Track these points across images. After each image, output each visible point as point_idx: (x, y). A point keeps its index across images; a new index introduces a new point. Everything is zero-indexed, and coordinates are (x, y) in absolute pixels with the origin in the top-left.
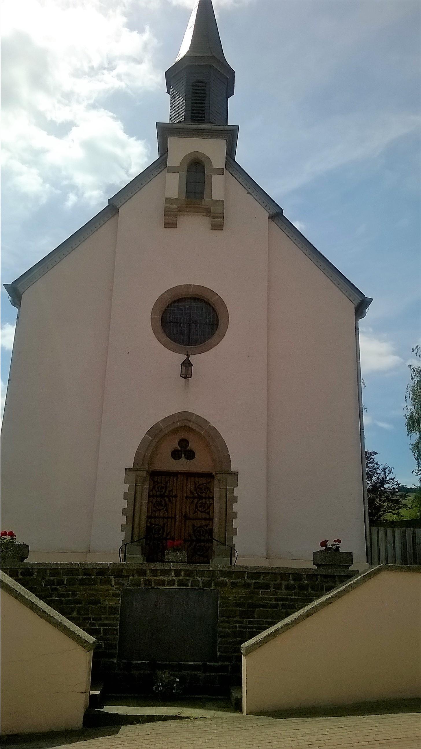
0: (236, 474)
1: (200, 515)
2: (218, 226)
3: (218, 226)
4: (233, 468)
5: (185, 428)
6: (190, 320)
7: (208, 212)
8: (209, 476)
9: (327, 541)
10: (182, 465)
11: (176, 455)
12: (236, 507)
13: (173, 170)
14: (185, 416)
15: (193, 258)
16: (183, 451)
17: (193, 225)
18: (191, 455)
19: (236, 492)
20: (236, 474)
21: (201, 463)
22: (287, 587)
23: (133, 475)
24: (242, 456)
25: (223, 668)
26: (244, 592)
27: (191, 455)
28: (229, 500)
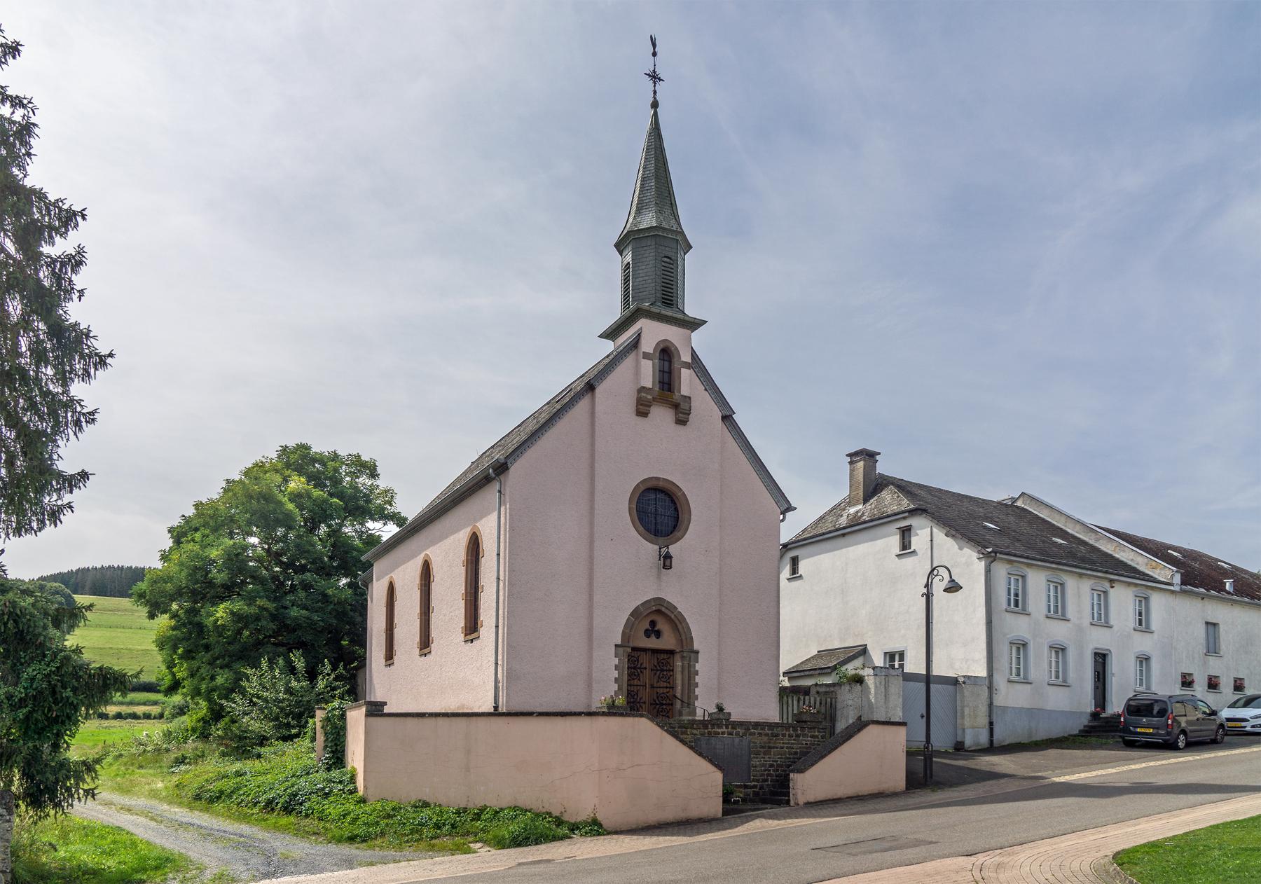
0: (697, 652)
1: (662, 684)
2: (682, 422)
3: (682, 422)
4: (695, 648)
5: (659, 612)
6: (660, 511)
7: (676, 406)
8: (672, 652)
9: (385, 704)
10: (652, 643)
11: (647, 634)
12: (697, 679)
13: (646, 356)
14: (659, 601)
15: (659, 450)
16: (653, 631)
17: (661, 416)
18: (658, 634)
19: (698, 667)
20: (697, 652)
21: (667, 641)
22: (790, 736)
23: (621, 650)
24: (701, 639)
25: (755, 786)
26: (766, 739)
27: (658, 634)
28: (691, 674)
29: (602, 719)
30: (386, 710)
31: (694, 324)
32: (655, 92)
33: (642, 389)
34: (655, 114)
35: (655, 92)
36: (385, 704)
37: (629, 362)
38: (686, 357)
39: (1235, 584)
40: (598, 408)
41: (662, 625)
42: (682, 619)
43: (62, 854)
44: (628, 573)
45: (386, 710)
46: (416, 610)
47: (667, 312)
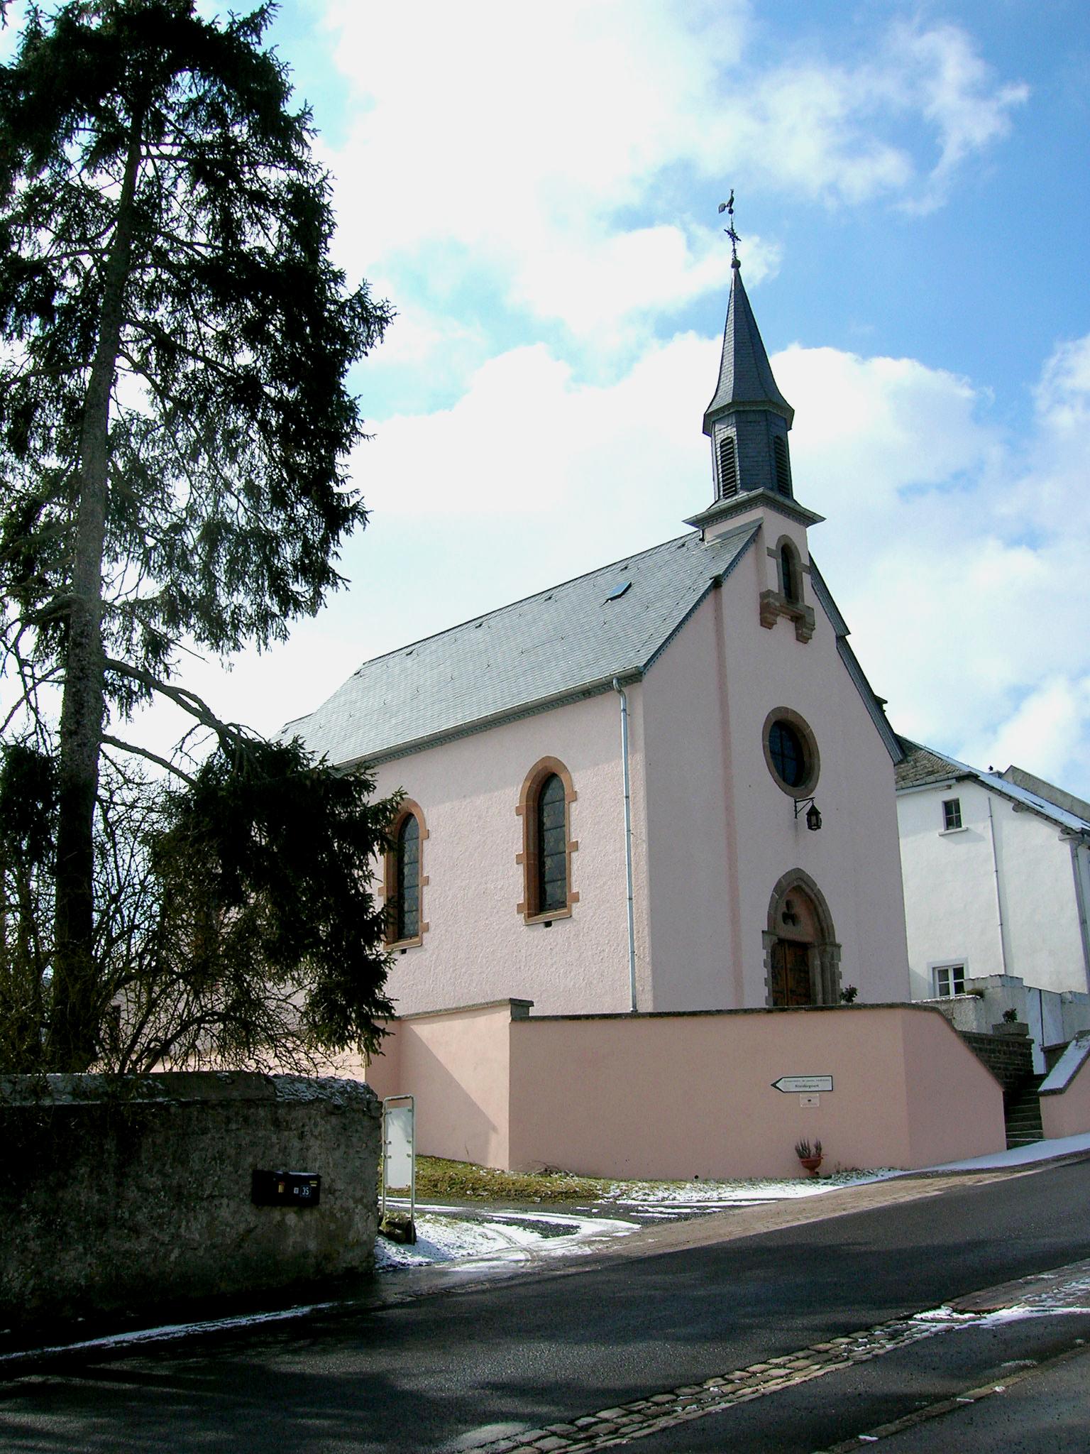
2: (803, 638)
5: (798, 889)
9: (531, 1004)
15: (777, 674)
21: (803, 931)
29: (953, 1035)
30: (533, 1012)
31: (809, 519)
32: (734, 251)
33: (765, 595)
34: (738, 277)
35: (734, 251)
36: (531, 1004)
37: (749, 557)
38: (806, 562)
39: (344, 994)
40: (727, 612)
41: (800, 910)
42: (822, 901)
43: (143, 1244)
44: (769, 838)
45: (533, 1012)
46: (1004, 790)
47: (780, 498)
